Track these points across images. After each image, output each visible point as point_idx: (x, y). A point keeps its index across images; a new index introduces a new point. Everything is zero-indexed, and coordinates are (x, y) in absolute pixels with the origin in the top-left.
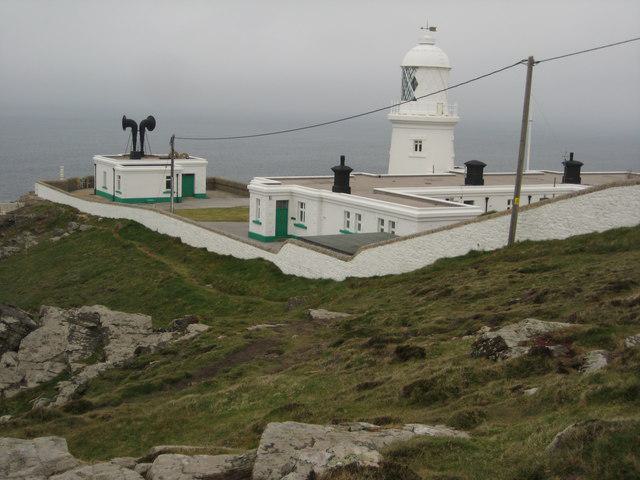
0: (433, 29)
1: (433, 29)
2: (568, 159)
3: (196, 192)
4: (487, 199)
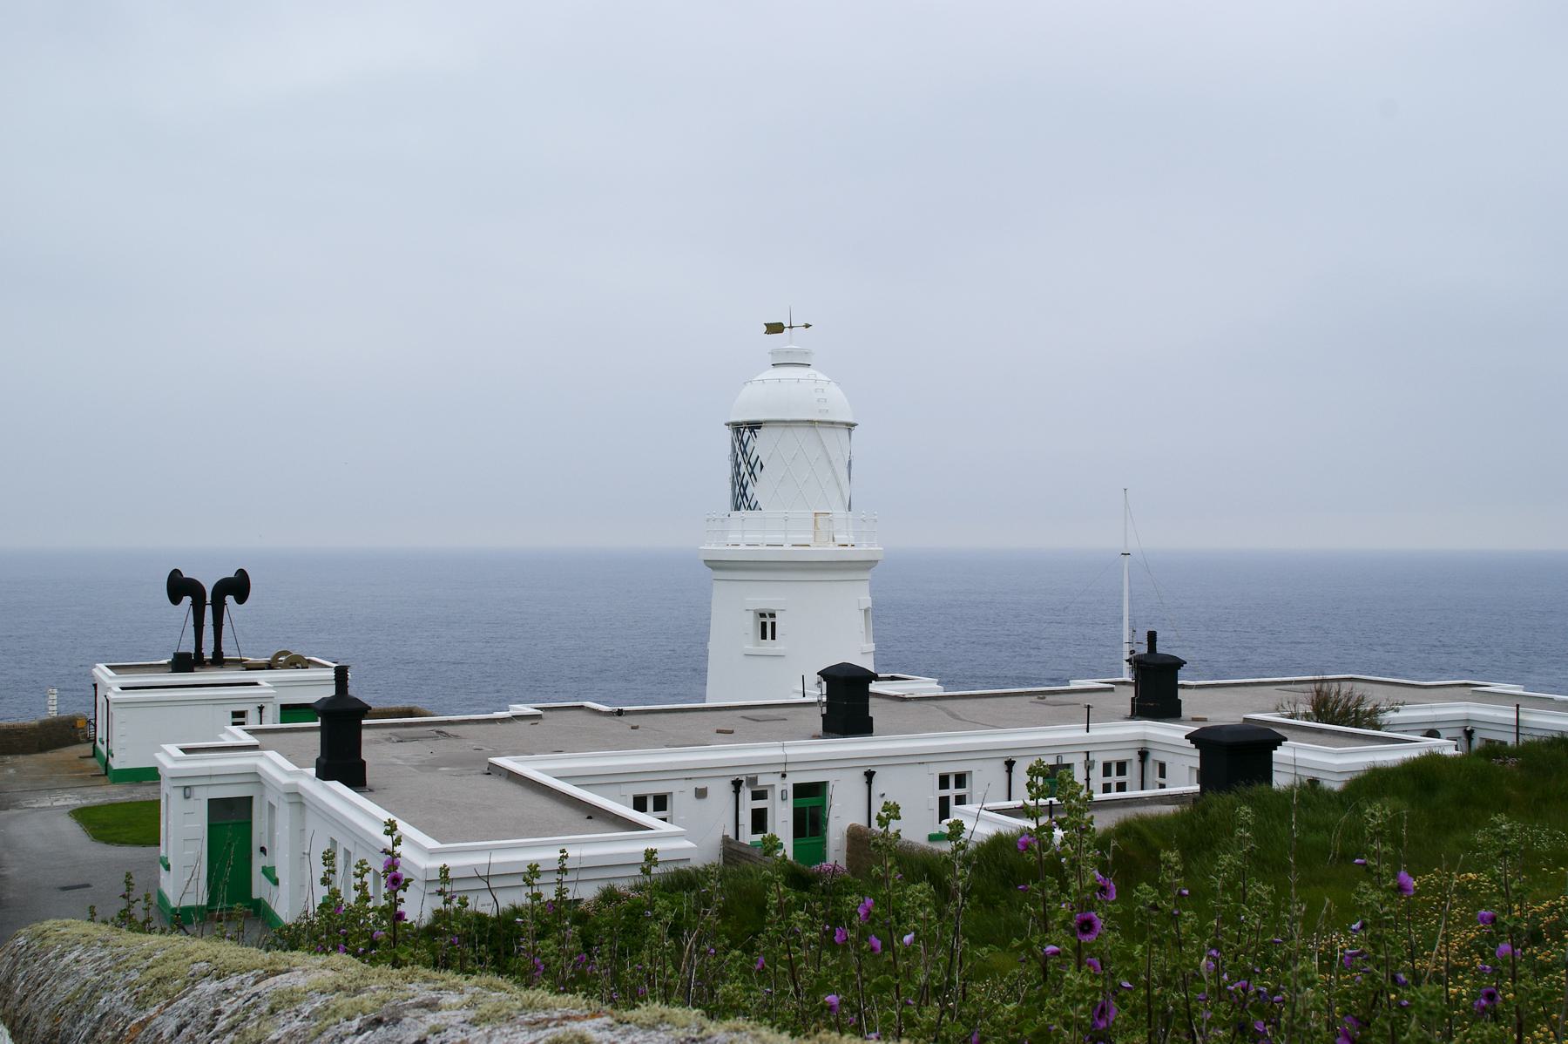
0: (807, 326)
1: (807, 326)
2: (1144, 650)
3: (116, 764)
4: (870, 775)
